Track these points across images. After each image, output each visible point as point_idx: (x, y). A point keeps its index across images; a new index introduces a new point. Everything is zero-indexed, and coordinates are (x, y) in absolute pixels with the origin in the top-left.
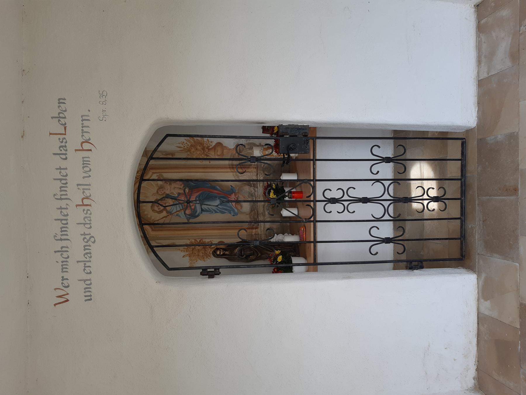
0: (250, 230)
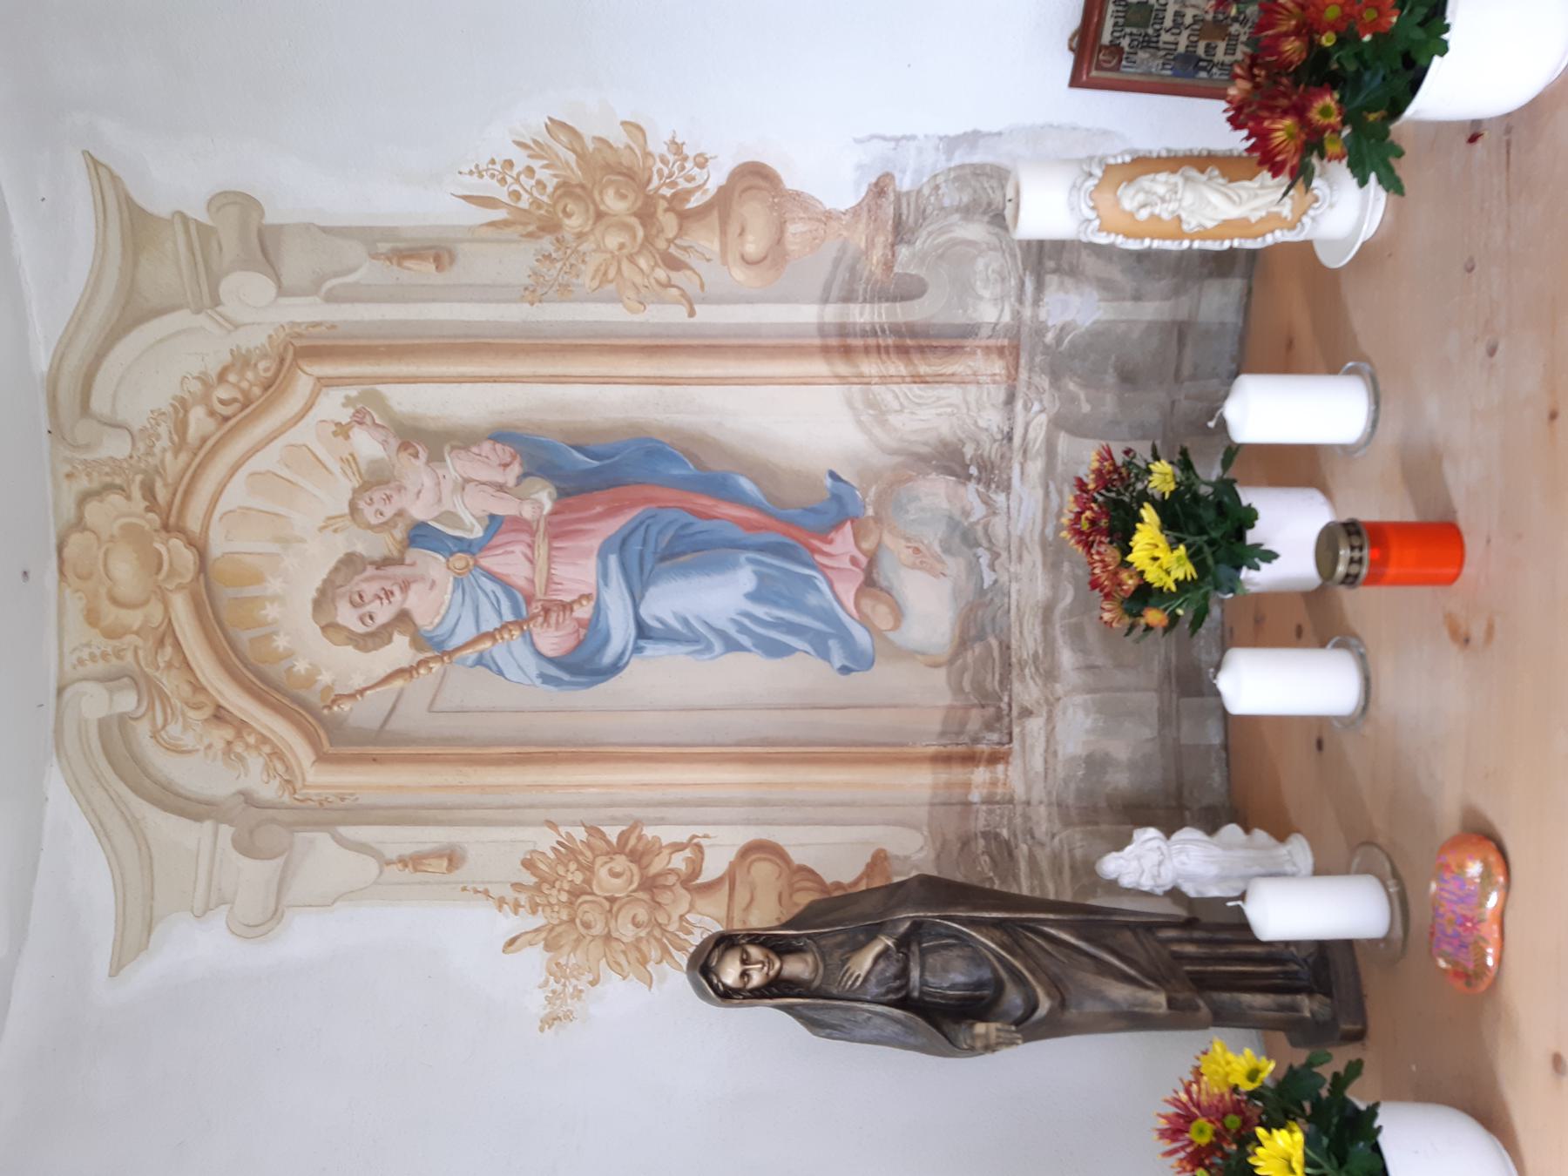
0: (957, 773)
